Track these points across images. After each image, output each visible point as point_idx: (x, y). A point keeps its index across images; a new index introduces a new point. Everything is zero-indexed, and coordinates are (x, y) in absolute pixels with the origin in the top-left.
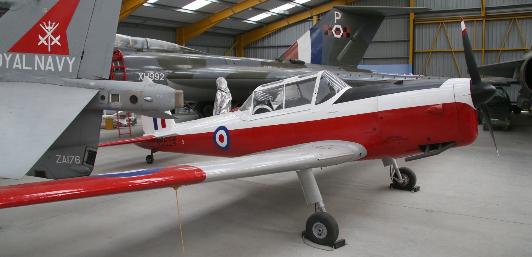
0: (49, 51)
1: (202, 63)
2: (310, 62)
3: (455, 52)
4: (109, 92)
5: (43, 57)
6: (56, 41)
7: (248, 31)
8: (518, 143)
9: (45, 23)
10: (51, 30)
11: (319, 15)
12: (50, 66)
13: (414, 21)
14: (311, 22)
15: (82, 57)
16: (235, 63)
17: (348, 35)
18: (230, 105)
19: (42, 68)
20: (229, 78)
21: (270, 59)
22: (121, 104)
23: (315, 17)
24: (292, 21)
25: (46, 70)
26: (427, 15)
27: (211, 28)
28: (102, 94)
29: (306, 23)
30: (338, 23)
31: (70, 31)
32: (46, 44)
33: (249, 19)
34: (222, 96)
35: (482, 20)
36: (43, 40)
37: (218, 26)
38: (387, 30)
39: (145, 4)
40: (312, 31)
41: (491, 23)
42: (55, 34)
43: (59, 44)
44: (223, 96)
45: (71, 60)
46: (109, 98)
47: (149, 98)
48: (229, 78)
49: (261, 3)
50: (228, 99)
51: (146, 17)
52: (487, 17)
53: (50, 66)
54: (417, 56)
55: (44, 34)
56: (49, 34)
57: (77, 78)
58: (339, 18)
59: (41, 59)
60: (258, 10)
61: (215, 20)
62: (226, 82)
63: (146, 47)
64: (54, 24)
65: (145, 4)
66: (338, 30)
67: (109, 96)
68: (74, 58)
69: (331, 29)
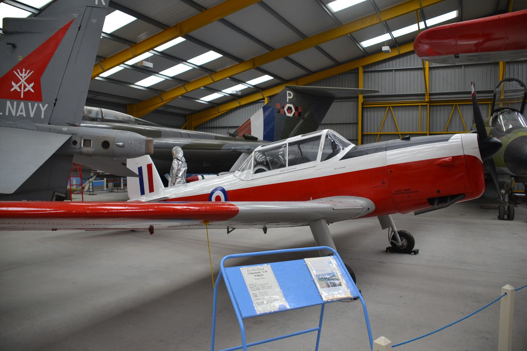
0: (22, 97)
1: (158, 134)
2: (262, 139)
3: (401, 134)
4: (81, 138)
5: (15, 103)
6: (29, 87)
7: (199, 111)
8: (461, 215)
9: (19, 71)
10: (25, 77)
11: (270, 97)
12: (22, 111)
13: (363, 104)
14: (262, 104)
15: (55, 104)
16: (189, 136)
17: (300, 114)
18: (185, 175)
19: (14, 113)
20: (184, 148)
21: (224, 134)
22: (93, 149)
23: (266, 99)
24: (243, 102)
25: (18, 115)
26: (374, 99)
27: (162, 106)
28: (74, 139)
29: (257, 105)
30: (290, 102)
31: (44, 79)
32: (19, 90)
33: (201, 99)
34: (179, 165)
35: (427, 105)
36: (16, 87)
37: (168, 104)
38: (337, 111)
39: (97, 78)
40: (265, 109)
41: (435, 108)
42: (28, 81)
43: (33, 91)
44: (179, 165)
45: (43, 107)
46: (81, 143)
47: (121, 144)
48: (184, 148)
49: (214, 82)
50: (184, 169)
51: (97, 92)
52: (430, 102)
53: (22, 111)
54: (365, 138)
55: (17, 81)
56: (23, 81)
57: (49, 124)
58: (291, 97)
59: (12, 105)
60: (211, 90)
61: (167, 98)
62: (182, 152)
63: (101, 117)
64: (28, 71)
65: (97, 78)
66: (289, 109)
67: (81, 141)
68: (47, 105)
69: (283, 108)
